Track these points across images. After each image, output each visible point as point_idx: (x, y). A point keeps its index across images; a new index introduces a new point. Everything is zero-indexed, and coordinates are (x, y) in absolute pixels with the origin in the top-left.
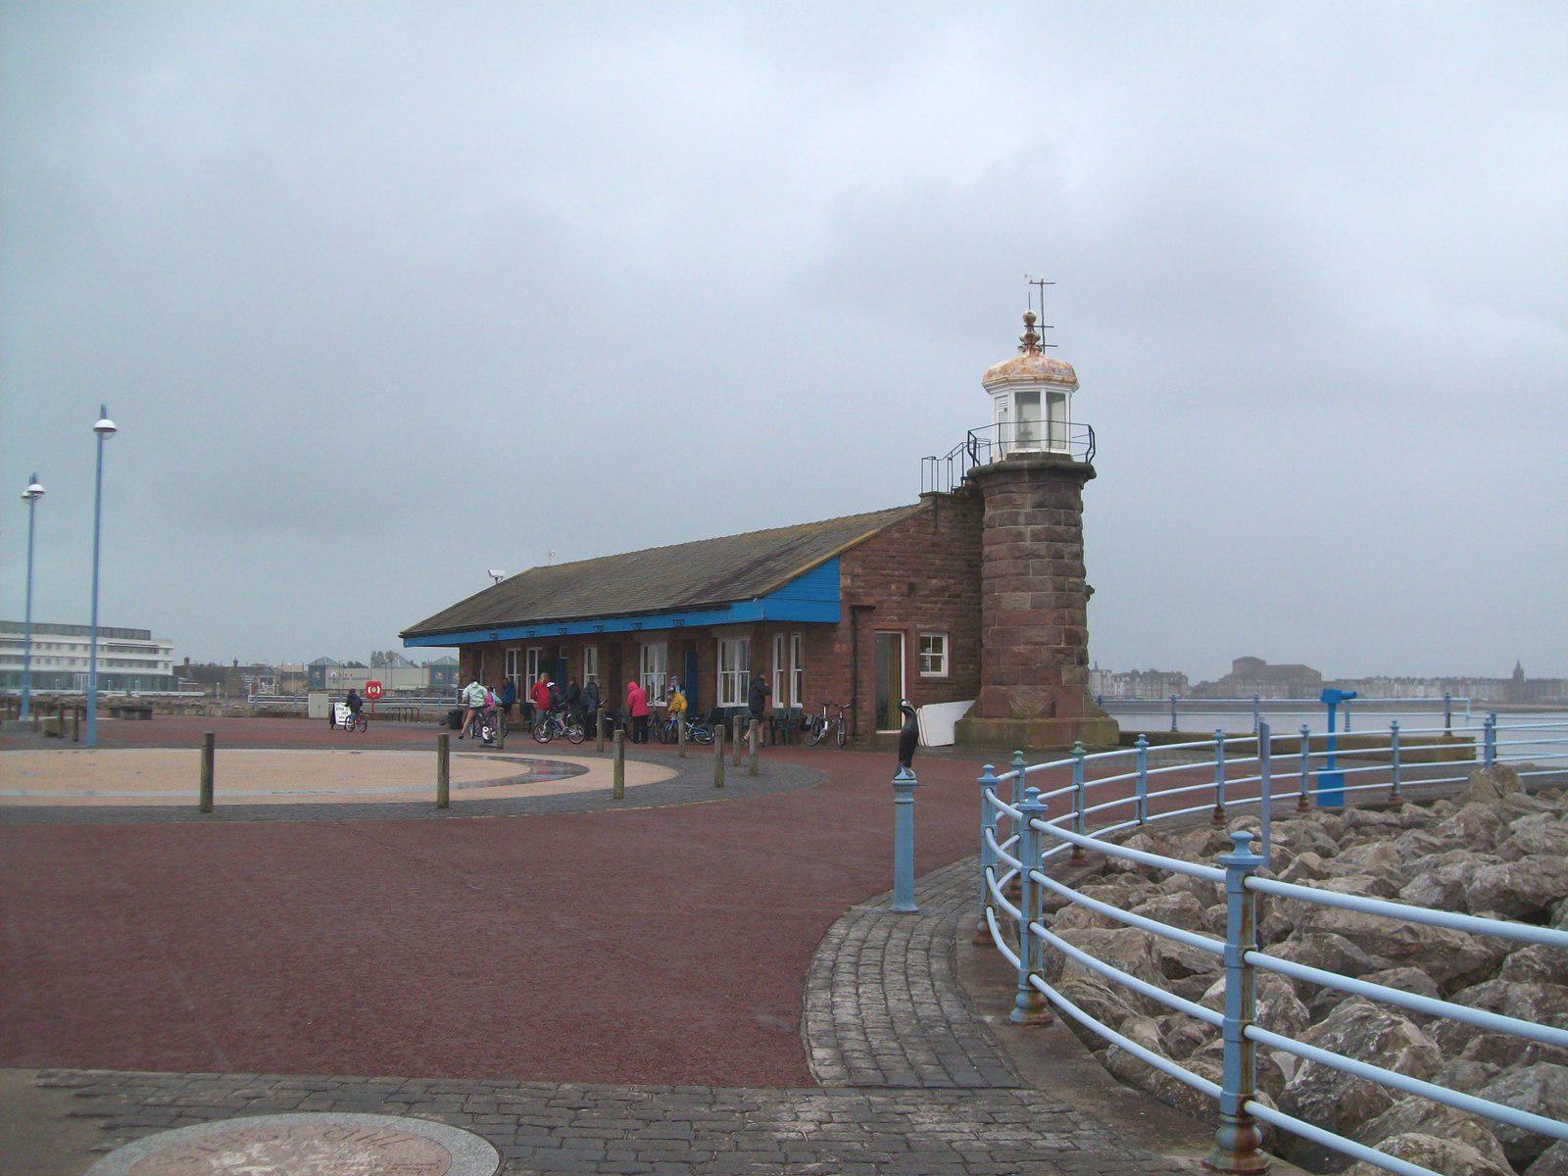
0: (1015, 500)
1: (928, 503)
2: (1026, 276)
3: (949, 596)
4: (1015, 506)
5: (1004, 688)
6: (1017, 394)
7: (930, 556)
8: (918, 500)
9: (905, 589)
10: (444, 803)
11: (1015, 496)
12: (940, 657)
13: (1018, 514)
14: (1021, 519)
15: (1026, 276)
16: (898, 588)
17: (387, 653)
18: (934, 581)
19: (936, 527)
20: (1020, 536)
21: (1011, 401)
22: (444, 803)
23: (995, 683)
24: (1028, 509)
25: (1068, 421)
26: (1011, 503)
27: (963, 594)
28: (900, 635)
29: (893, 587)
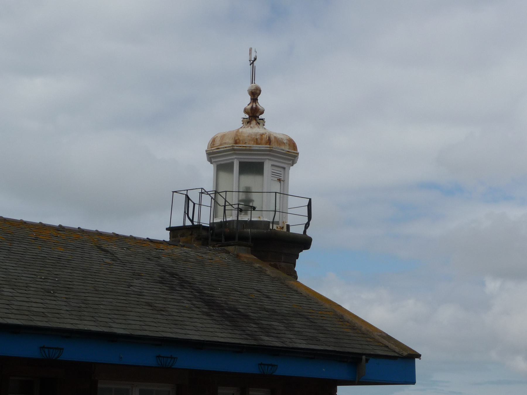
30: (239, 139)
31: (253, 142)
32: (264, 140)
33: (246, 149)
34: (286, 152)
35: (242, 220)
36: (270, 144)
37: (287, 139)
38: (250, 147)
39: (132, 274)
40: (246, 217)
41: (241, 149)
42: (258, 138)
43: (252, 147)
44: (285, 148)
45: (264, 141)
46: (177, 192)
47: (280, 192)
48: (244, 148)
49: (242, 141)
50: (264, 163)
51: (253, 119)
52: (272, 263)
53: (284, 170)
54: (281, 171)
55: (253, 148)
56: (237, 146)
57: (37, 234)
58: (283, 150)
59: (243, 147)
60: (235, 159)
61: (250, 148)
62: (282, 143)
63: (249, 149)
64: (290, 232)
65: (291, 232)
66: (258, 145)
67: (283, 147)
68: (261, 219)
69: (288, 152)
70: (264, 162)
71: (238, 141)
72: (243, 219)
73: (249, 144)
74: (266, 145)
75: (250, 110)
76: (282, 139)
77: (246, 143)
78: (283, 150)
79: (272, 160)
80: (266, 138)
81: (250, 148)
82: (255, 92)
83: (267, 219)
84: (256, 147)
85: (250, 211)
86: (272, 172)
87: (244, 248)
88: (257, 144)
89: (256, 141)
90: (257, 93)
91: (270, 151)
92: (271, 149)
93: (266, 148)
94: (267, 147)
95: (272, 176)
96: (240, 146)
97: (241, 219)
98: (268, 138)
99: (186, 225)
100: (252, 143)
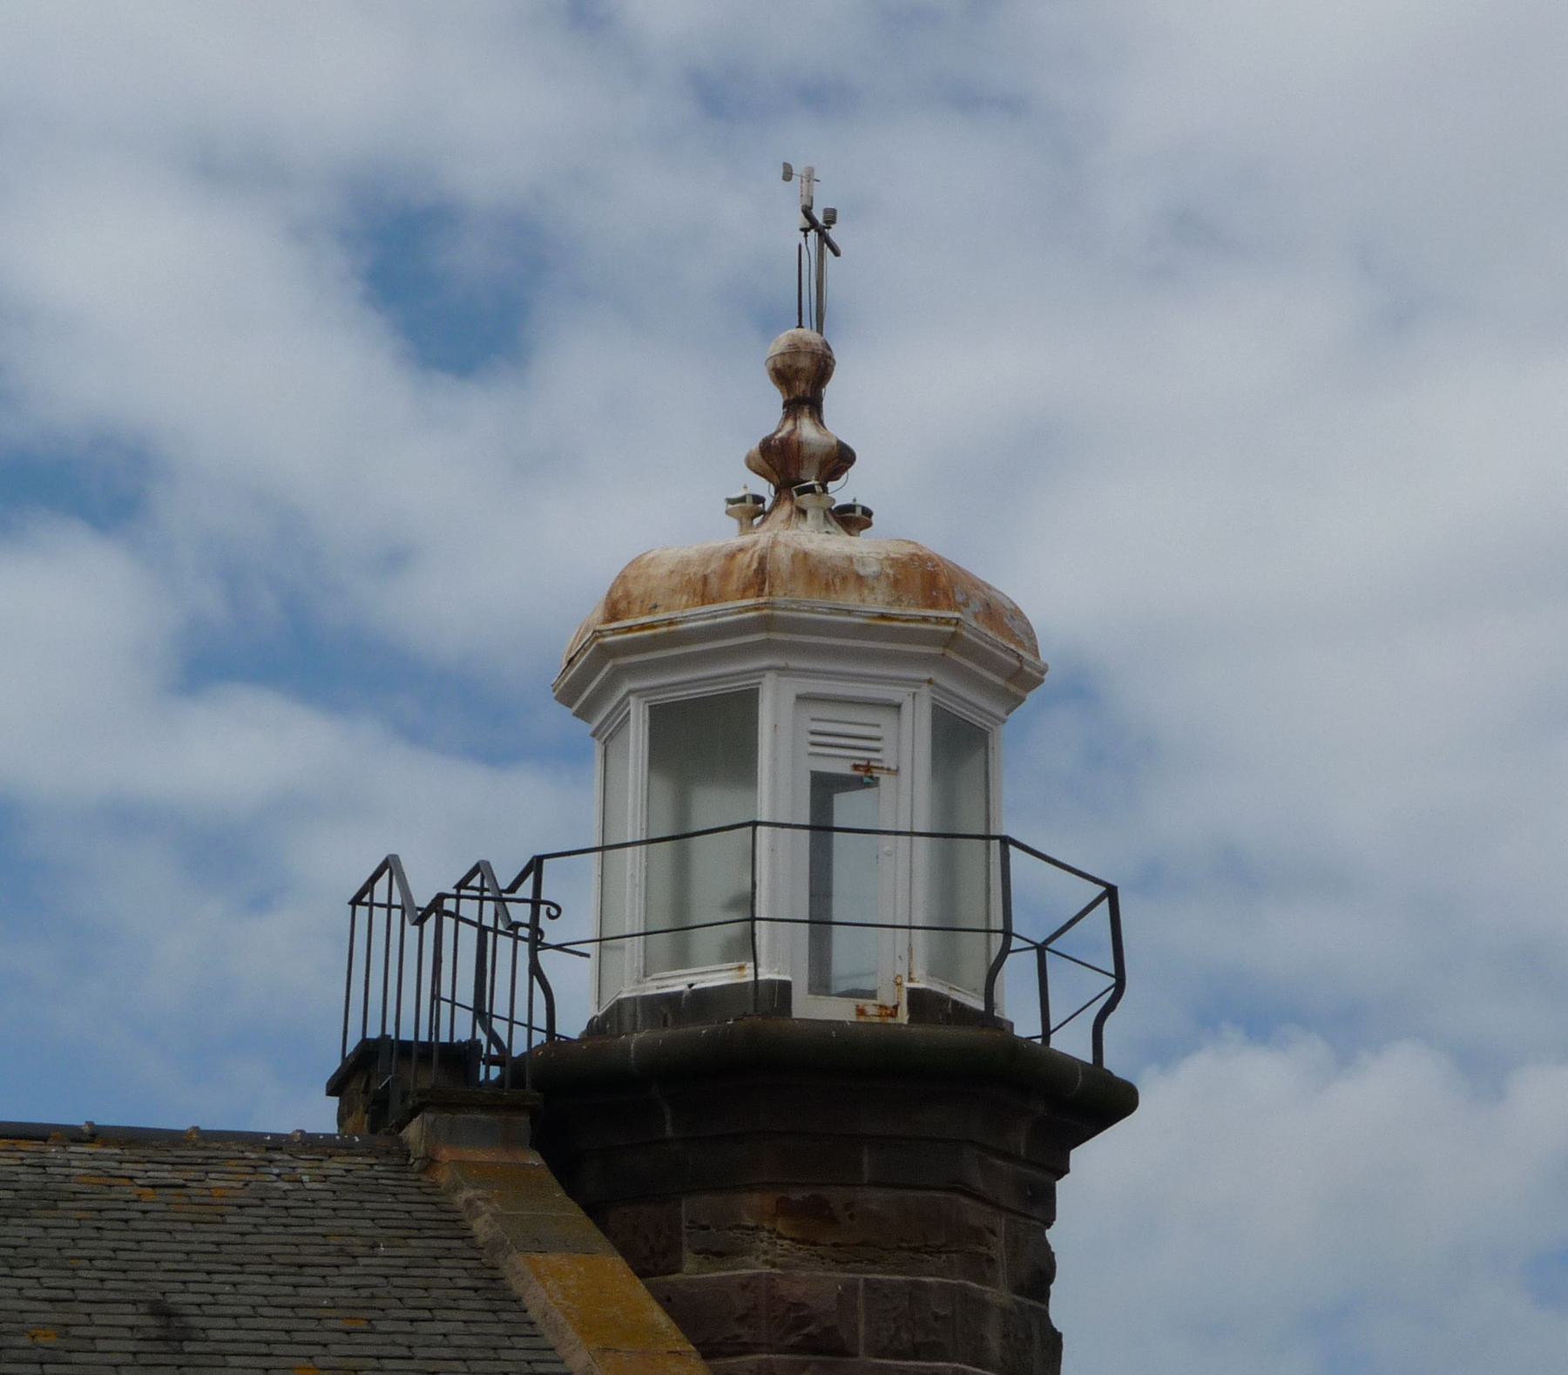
30: (627, 595)
31: (685, 597)
32: (735, 577)
33: (655, 636)
34: (874, 618)
35: (660, 995)
36: (763, 590)
37: (892, 555)
38: (671, 622)
39: (462, 1303)
40: (680, 976)
41: (635, 638)
42: (714, 572)
43: (681, 622)
44: (863, 601)
45: (734, 583)
46: (1032, 945)
47: (909, 830)
48: (647, 633)
49: (639, 603)
50: (760, 691)
51: (783, 497)
52: (797, 1196)
53: (899, 719)
54: (878, 726)
55: (681, 627)
56: (615, 631)
57: (318, 1168)
58: (849, 612)
59: (643, 627)
60: (632, 699)
61: (673, 628)
62: (844, 579)
63: (671, 633)
64: (1051, 1046)
65: (1051, 1046)
66: (709, 603)
67: (850, 599)
68: (745, 976)
69: (883, 617)
70: (758, 689)
71: (622, 605)
72: (667, 986)
73: (668, 609)
74: (742, 598)
75: (760, 456)
76: (850, 559)
77: (655, 607)
78: (849, 612)
79: (798, 670)
80: (749, 566)
81: (673, 628)
82: (790, 367)
83: (779, 973)
84: (697, 616)
85: (367, 908)
86: (813, 733)
87: (483, 1117)
88: (705, 599)
89: (699, 587)
90: (797, 371)
91: (766, 623)
92: (765, 612)
93: (740, 612)
94: (747, 609)
95: (811, 754)
96: (630, 629)
97: (658, 988)
98: (755, 565)
99: (401, 1038)
100: (684, 602)
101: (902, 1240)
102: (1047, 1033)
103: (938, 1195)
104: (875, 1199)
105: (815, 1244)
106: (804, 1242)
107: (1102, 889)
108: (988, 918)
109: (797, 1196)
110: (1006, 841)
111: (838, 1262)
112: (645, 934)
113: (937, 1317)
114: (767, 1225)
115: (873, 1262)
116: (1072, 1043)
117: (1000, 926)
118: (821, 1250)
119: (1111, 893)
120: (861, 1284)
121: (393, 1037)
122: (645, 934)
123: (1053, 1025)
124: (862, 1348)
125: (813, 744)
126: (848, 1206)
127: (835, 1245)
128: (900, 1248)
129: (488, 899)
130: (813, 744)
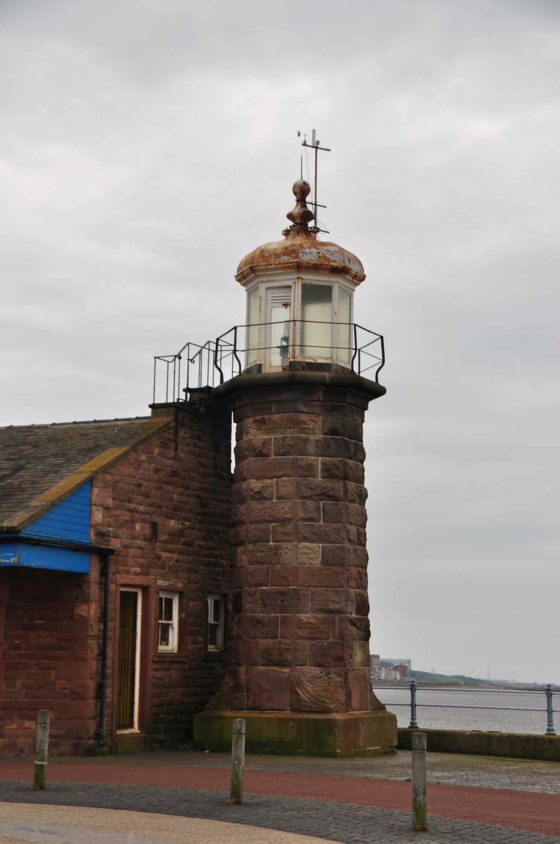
0: (304, 423)
1: (167, 418)
2: (299, 134)
3: (185, 544)
4: (303, 430)
5: (286, 670)
6: (304, 286)
7: (170, 488)
8: (148, 412)
9: (148, 530)
10: (547, 711)
11: (304, 417)
12: (168, 625)
13: (306, 441)
14: (311, 448)
15: (299, 134)
16: (142, 528)
17: (322, 565)
18: (172, 523)
19: (176, 450)
20: (309, 469)
21: (297, 293)
22: (547, 711)
23: (272, 663)
24: (320, 436)
25: (298, 324)
26: (298, 424)
27: (196, 542)
28: (136, 594)
29: (138, 527)
52: (258, 418)
86: (272, 297)
101: (282, 426)
102: (359, 372)
103: (291, 414)
104: (276, 417)
105: (261, 430)
106: (258, 429)
107: (379, 337)
108: (350, 343)
109: (258, 418)
110: (355, 325)
111: (267, 434)
112: (271, 348)
113: (289, 445)
114: (251, 426)
115: (275, 432)
116: (368, 375)
117: (354, 347)
118: (262, 431)
119: (382, 338)
120: (273, 438)
121: (357, 374)
122: (271, 348)
123: (361, 371)
124: (272, 454)
125: (272, 300)
126: (269, 419)
127: (266, 429)
128: (281, 428)
129: (333, 336)
130: (272, 300)
